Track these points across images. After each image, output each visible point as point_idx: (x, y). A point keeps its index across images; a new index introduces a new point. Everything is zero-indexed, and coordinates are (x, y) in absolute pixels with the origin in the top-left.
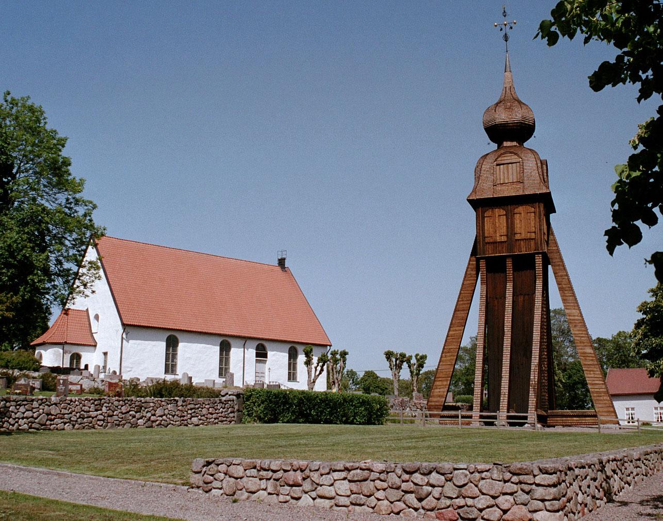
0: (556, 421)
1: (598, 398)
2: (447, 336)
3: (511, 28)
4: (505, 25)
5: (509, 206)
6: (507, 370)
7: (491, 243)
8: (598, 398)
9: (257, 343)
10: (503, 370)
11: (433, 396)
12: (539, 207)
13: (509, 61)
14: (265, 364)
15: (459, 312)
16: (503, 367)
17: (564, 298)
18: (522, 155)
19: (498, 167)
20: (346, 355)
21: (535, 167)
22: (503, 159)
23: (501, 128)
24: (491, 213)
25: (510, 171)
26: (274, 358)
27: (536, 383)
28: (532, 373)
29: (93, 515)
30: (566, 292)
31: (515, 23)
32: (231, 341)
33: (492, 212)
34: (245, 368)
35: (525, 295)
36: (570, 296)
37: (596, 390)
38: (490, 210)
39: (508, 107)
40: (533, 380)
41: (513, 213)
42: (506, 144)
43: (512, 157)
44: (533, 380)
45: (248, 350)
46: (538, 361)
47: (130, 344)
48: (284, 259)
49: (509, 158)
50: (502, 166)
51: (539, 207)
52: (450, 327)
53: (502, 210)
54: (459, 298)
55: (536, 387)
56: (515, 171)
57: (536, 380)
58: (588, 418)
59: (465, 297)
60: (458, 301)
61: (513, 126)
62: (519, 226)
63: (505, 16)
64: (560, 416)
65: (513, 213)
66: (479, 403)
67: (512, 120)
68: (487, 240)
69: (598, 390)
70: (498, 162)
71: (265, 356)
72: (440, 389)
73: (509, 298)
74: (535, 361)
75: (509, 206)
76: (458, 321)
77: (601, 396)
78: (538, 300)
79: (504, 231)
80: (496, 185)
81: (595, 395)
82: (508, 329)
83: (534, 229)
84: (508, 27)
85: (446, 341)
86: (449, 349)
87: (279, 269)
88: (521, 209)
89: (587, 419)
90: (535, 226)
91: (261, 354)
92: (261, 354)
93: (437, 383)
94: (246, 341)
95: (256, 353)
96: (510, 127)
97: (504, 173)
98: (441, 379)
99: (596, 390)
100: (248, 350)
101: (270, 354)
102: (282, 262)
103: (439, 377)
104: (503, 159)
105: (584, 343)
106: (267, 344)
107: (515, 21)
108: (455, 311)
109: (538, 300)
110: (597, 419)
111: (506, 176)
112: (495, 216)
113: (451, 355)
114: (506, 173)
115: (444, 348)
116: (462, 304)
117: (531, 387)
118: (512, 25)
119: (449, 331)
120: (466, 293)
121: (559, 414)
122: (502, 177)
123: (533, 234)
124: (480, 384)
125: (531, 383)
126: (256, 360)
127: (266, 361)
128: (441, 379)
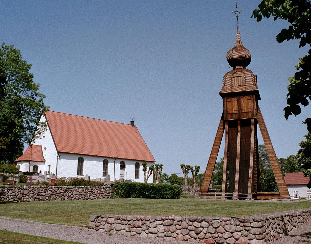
0: (261, 197)
1: (280, 186)
2: (210, 157)
3: (240, 13)
4: (237, 12)
5: (239, 96)
6: (238, 173)
7: (231, 114)
8: (280, 186)
9: (121, 160)
10: (236, 173)
11: (203, 186)
12: (253, 97)
13: (239, 28)
14: (125, 170)
15: (215, 146)
16: (236, 172)
17: (265, 139)
18: (245, 73)
19: (234, 78)
20: (162, 166)
21: (251, 78)
22: (236, 74)
23: (235, 60)
24: (230, 100)
25: (239, 80)
26: (129, 168)
27: (252, 179)
28: (249, 175)
29: (43, 241)
30: (265, 137)
31: (242, 11)
32: (108, 160)
33: (231, 99)
34: (115, 172)
35: (246, 138)
36: (268, 139)
37: (280, 183)
38: (230, 98)
39: (238, 50)
40: (250, 178)
41: (240, 100)
42: (237, 67)
43: (240, 74)
44: (250, 178)
45: (116, 164)
46: (252, 169)
47: (61, 161)
48: (133, 121)
49: (239, 74)
50: (235, 78)
51: (253, 97)
52: (211, 153)
53: (235, 99)
54: (215, 140)
55: (251, 181)
56: (242, 80)
57: (252, 178)
58: (276, 196)
59: (218, 139)
60: (215, 141)
61: (241, 59)
62: (243, 106)
63: (237, 8)
64: (263, 195)
65: (240, 100)
66: (225, 189)
67: (240, 56)
68: (228, 112)
69: (281, 183)
70: (234, 76)
71: (124, 167)
72: (206, 182)
73: (239, 140)
74: (251, 169)
75: (239, 96)
76: (215, 150)
77: (282, 186)
78: (252, 141)
79: (236, 108)
80: (232, 87)
81: (279, 185)
82: (238, 154)
83: (250, 107)
84: (238, 13)
85: (209, 160)
86: (211, 163)
87: (131, 126)
88: (244, 98)
89: (275, 196)
90: (251, 106)
91: (123, 166)
92: (123, 166)
93: (205, 179)
94: (115, 160)
95: (120, 165)
96: (239, 60)
97: (236, 81)
98: (207, 178)
99: (280, 183)
100: (116, 164)
101: (126, 166)
102: (132, 123)
103: (206, 177)
104: (236, 74)
105: (274, 161)
106: (125, 161)
107: (242, 10)
108: (214, 145)
109: (252, 141)
110: (280, 196)
111: (237, 82)
112: (232, 101)
113: (212, 166)
114: (237, 81)
115: (208, 163)
116: (217, 142)
117: (249, 181)
118: (240, 12)
119: (211, 155)
120: (219, 137)
121: (262, 194)
122: (235, 83)
123: (250, 110)
124: (225, 180)
125: (249, 179)
126: (120, 168)
127: (125, 169)
128: (207, 178)
